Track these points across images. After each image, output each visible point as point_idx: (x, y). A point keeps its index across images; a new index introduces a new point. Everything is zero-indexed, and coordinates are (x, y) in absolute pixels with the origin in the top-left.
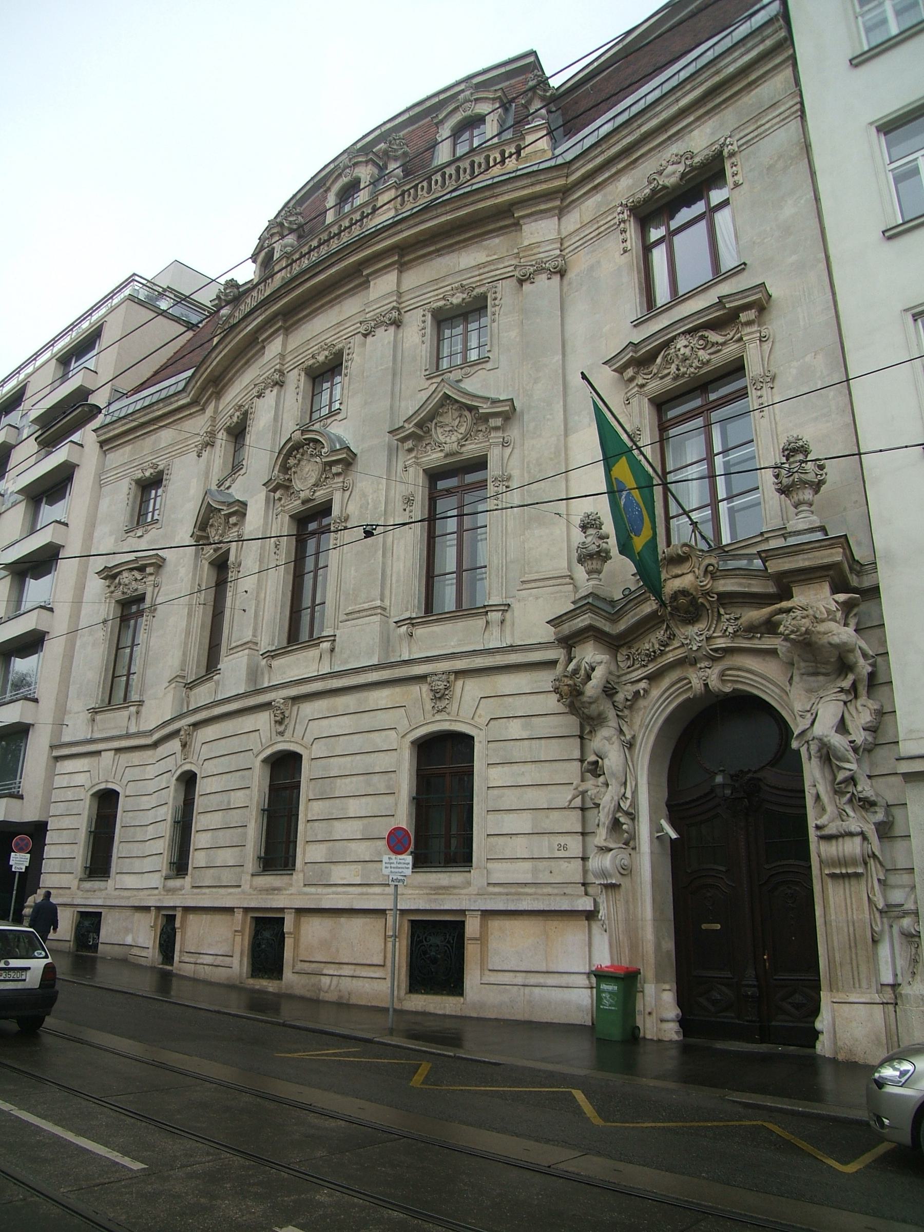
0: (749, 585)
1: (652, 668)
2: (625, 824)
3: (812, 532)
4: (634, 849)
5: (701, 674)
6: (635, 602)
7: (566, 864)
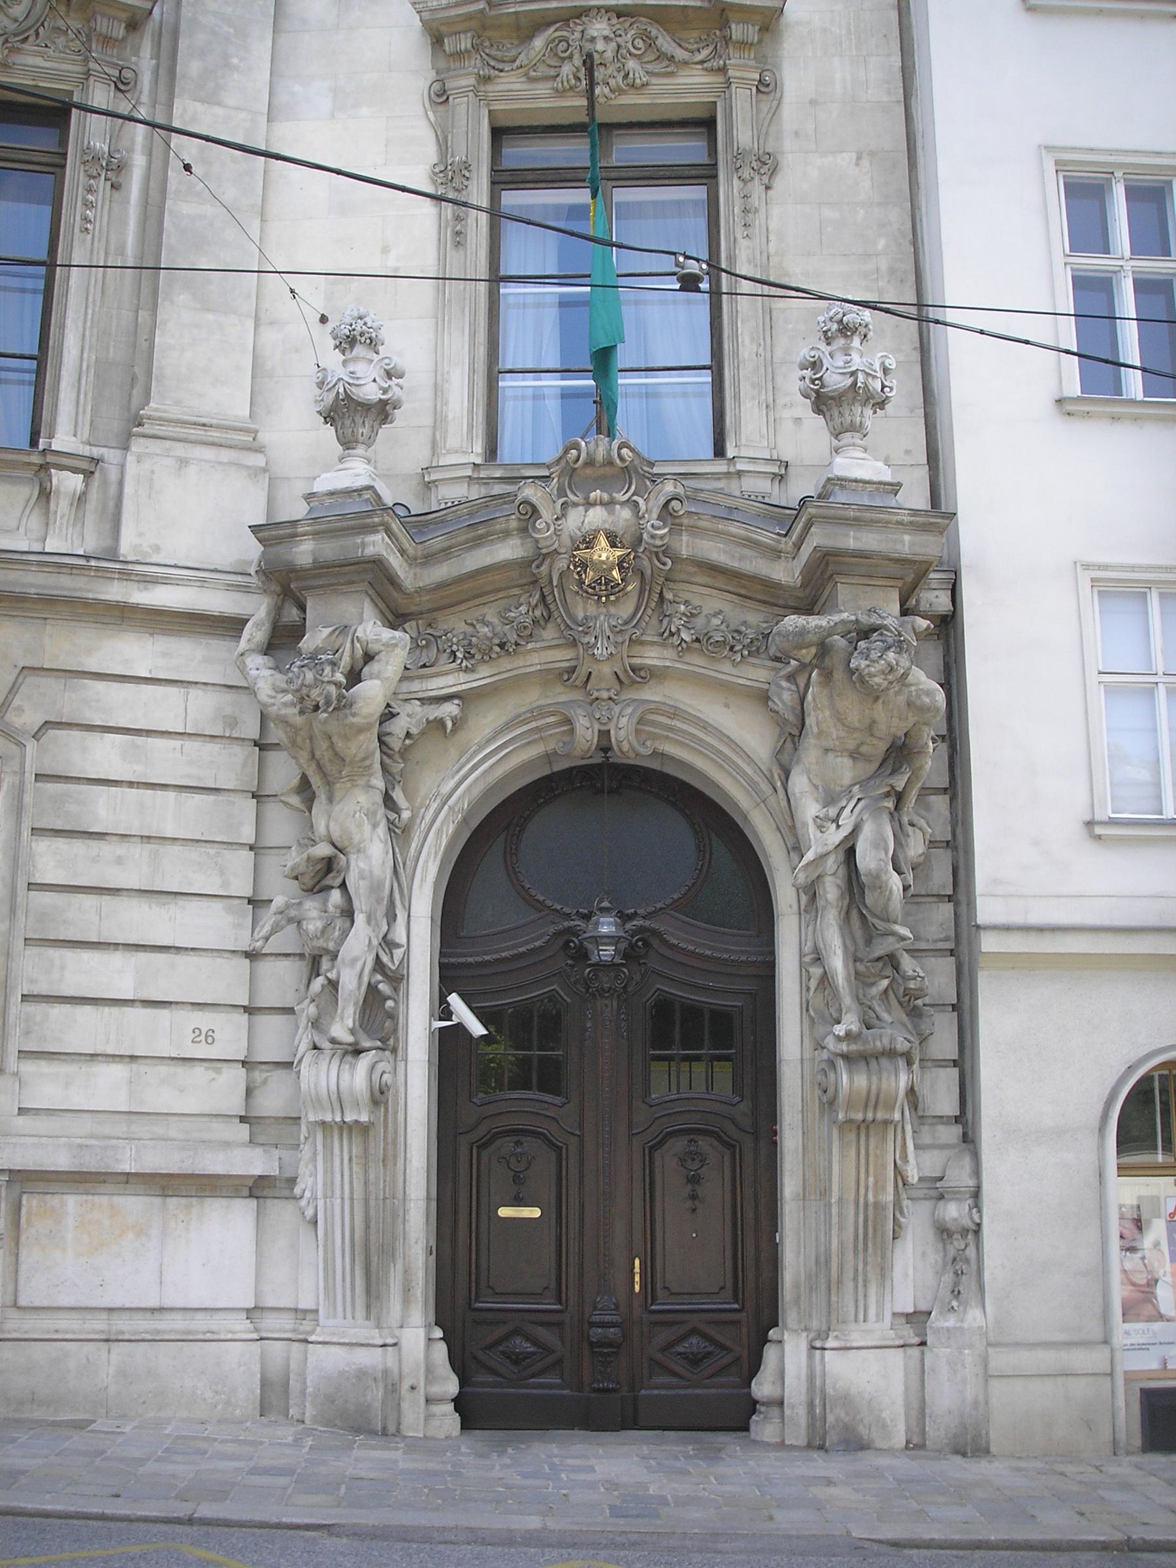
2: (389, 998)
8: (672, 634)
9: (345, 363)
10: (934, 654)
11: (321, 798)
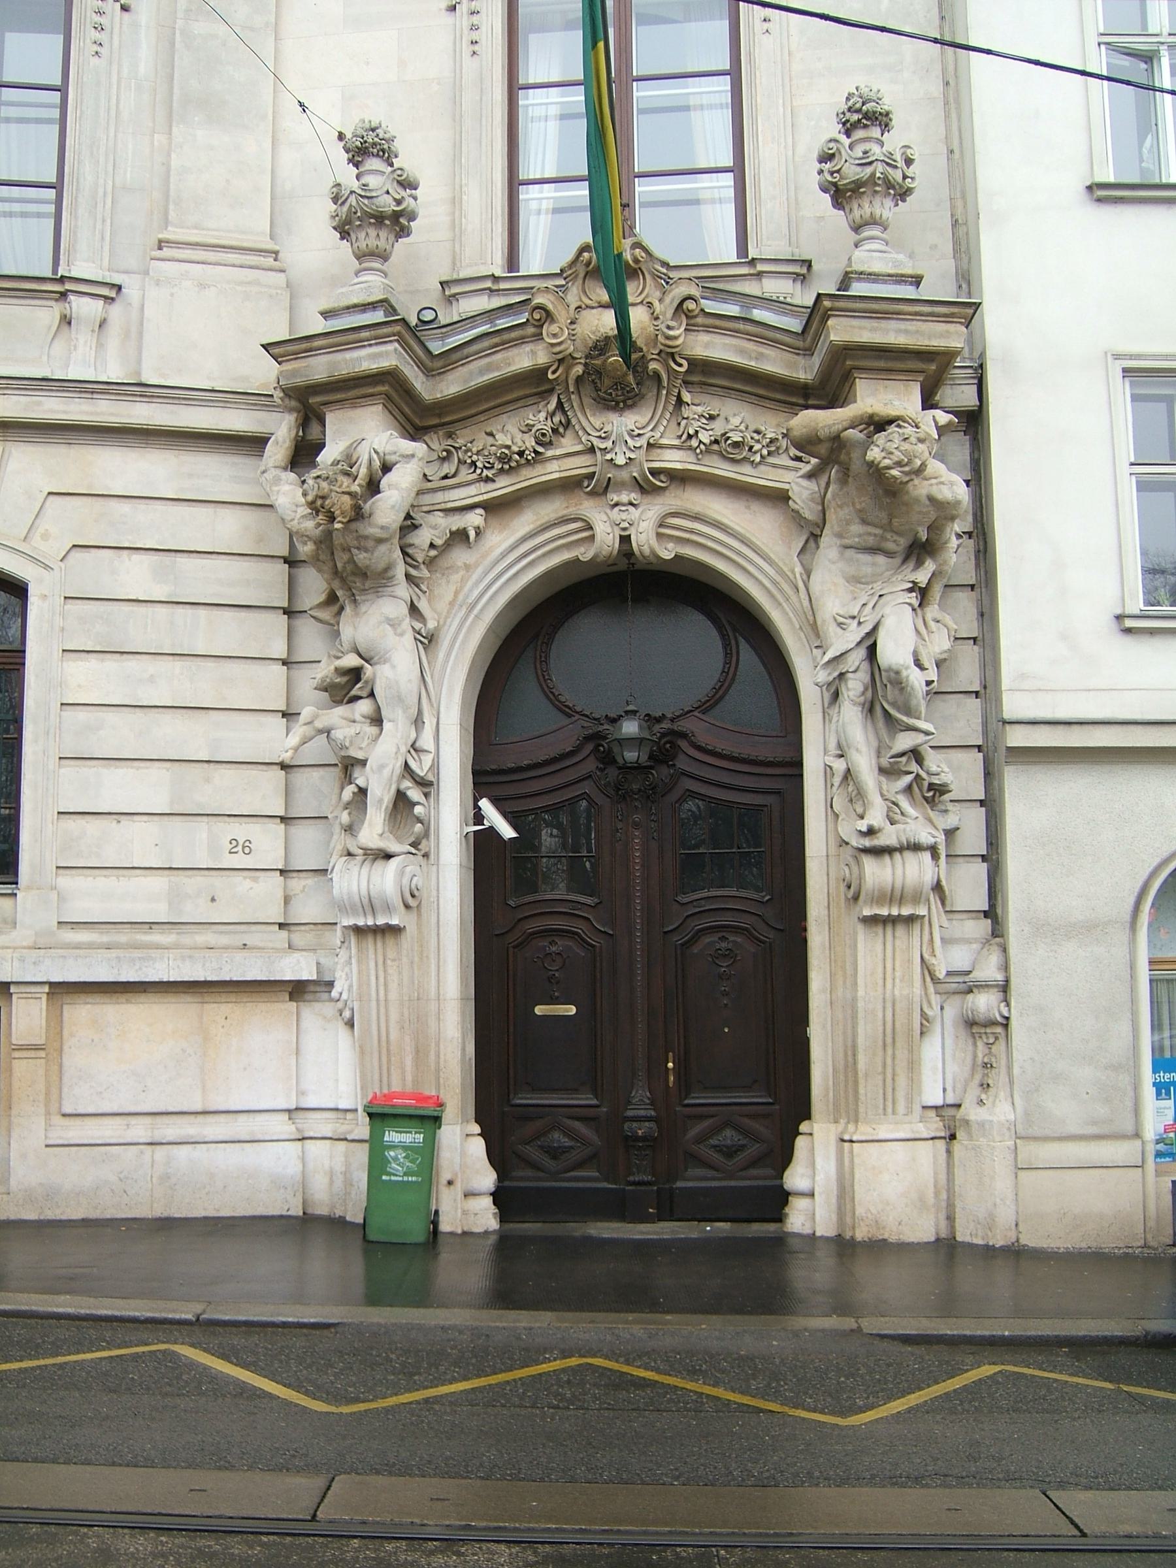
0: (760, 357)
1: (504, 486)
2: (418, 803)
3: (899, 282)
4: (426, 856)
5: (615, 514)
6: (496, 340)
7: (248, 883)
8: (690, 437)
9: (358, 177)
10: (960, 448)
11: (348, 609)
